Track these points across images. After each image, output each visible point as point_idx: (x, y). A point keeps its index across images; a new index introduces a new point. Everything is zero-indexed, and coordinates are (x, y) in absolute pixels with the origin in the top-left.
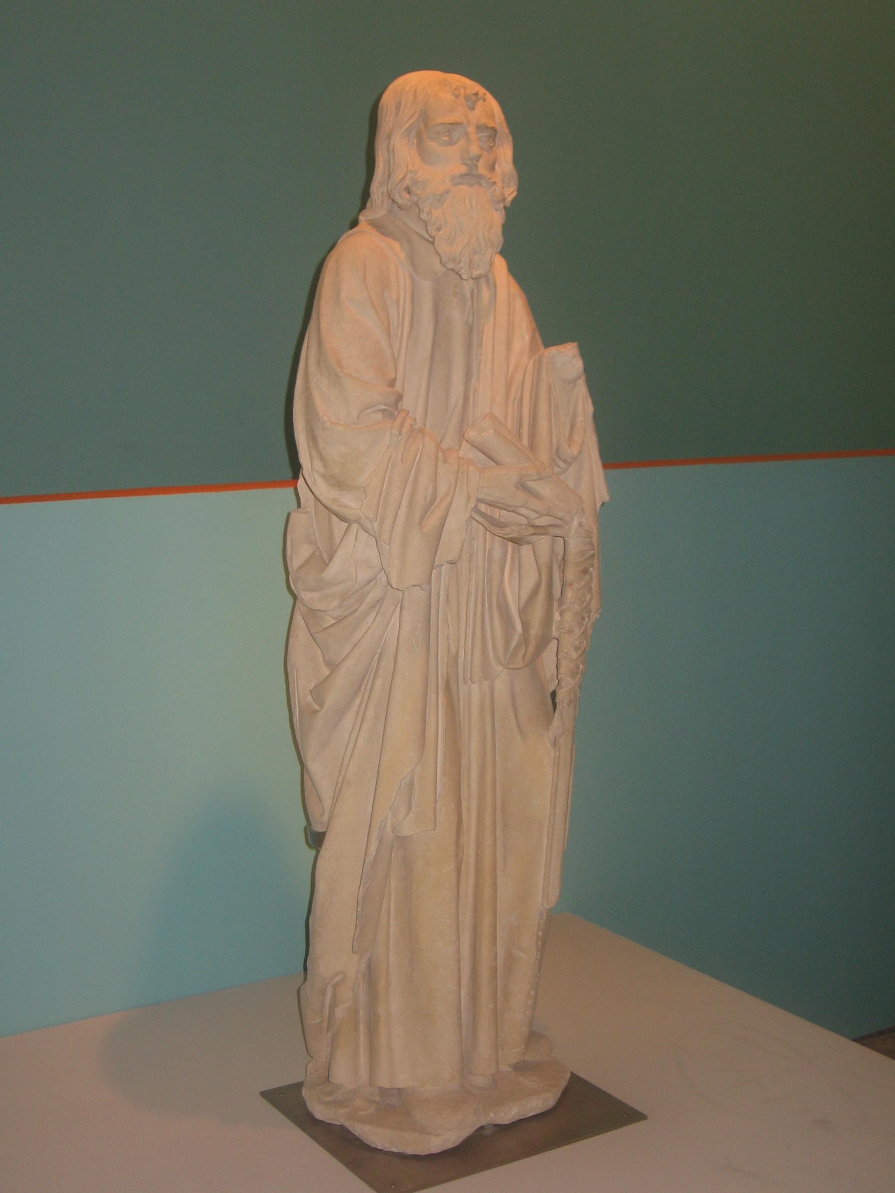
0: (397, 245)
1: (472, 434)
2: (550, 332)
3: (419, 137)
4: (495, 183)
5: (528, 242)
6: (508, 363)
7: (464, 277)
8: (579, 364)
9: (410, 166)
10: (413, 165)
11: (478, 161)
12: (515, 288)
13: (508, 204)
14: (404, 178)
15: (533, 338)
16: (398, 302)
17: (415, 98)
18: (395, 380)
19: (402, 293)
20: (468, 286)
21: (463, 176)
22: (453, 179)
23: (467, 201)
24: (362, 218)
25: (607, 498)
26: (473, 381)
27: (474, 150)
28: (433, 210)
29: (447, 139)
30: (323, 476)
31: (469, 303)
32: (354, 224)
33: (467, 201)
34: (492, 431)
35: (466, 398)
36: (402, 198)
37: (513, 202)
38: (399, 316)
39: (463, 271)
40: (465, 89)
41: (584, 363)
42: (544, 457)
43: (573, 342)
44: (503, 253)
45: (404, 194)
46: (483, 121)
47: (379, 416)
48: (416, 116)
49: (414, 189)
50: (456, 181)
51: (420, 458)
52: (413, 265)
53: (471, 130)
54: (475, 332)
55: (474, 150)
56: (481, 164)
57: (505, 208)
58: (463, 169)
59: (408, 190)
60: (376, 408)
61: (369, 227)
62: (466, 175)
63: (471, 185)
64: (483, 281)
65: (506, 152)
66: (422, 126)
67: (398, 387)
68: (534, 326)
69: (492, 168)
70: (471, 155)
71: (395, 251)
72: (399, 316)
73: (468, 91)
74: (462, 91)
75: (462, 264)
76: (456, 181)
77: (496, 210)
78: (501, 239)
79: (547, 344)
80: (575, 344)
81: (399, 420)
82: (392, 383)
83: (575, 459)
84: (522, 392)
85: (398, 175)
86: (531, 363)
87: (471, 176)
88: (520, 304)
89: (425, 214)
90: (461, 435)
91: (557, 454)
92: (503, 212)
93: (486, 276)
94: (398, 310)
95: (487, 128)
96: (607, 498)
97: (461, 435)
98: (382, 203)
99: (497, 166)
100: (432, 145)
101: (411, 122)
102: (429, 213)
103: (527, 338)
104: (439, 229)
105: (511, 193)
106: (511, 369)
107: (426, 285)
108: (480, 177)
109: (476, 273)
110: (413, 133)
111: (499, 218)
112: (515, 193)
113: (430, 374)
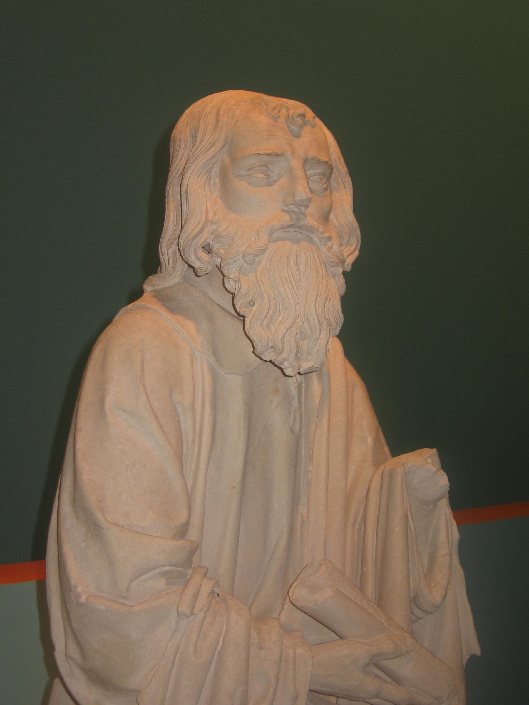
0: (191, 326)
1: (300, 593)
2: (400, 432)
3: (224, 175)
4: (330, 239)
5: (380, 325)
6: (346, 479)
7: (288, 372)
8: (443, 481)
9: (211, 215)
10: (215, 213)
11: (307, 207)
12: (459, 573)
13: (348, 268)
14: (202, 230)
15: (376, 440)
16: (193, 406)
17: (217, 120)
18: (187, 523)
19: (199, 394)
20: (292, 383)
21: (284, 228)
22: (271, 234)
23: (292, 263)
24: (147, 288)
25: (477, 651)
26: (302, 509)
27: (302, 193)
28: (242, 277)
29: (261, 176)
30: (82, 668)
31: (295, 403)
32: (136, 294)
33: (292, 263)
34: (329, 592)
35: (292, 529)
36: (200, 260)
37: (355, 264)
38: (195, 430)
39: (286, 364)
40: (288, 109)
41: (450, 480)
42: (400, 613)
43: (431, 447)
44: (340, 336)
45: (204, 256)
46: (312, 153)
47: (161, 583)
48: (219, 145)
49: (217, 246)
50: (276, 235)
51: (223, 645)
52: (215, 353)
53: (295, 163)
54: (303, 441)
55: (302, 193)
56: (312, 210)
57: (344, 273)
58: (286, 219)
59: (208, 249)
60: (157, 571)
61: (154, 300)
62: (291, 226)
63: (297, 241)
64: (314, 377)
65: (344, 197)
66: (227, 160)
67: (193, 534)
68: (376, 423)
69: (325, 218)
70: (298, 198)
71: (189, 334)
72: (195, 430)
73: (292, 112)
74: (284, 111)
75: (284, 355)
76: (276, 235)
77: (334, 276)
78: (341, 318)
79: (396, 452)
80: (434, 450)
81: (191, 590)
82: (182, 532)
83: (438, 607)
84: (365, 511)
85: (192, 227)
86: (377, 478)
87: (294, 228)
88: (360, 394)
89: (232, 283)
90: (285, 588)
91: (414, 600)
92: (342, 280)
93: (318, 371)
94: (194, 416)
95: (319, 162)
96: (477, 651)
97: (285, 588)
98: (174, 267)
99: (332, 216)
100: (241, 185)
101: (210, 153)
102: (237, 281)
103: (370, 440)
104: (251, 304)
105: (351, 252)
106: (351, 476)
107: (234, 384)
108: (309, 229)
109: (305, 366)
110: (216, 170)
111: (337, 286)
112: (357, 253)
113: (240, 507)
